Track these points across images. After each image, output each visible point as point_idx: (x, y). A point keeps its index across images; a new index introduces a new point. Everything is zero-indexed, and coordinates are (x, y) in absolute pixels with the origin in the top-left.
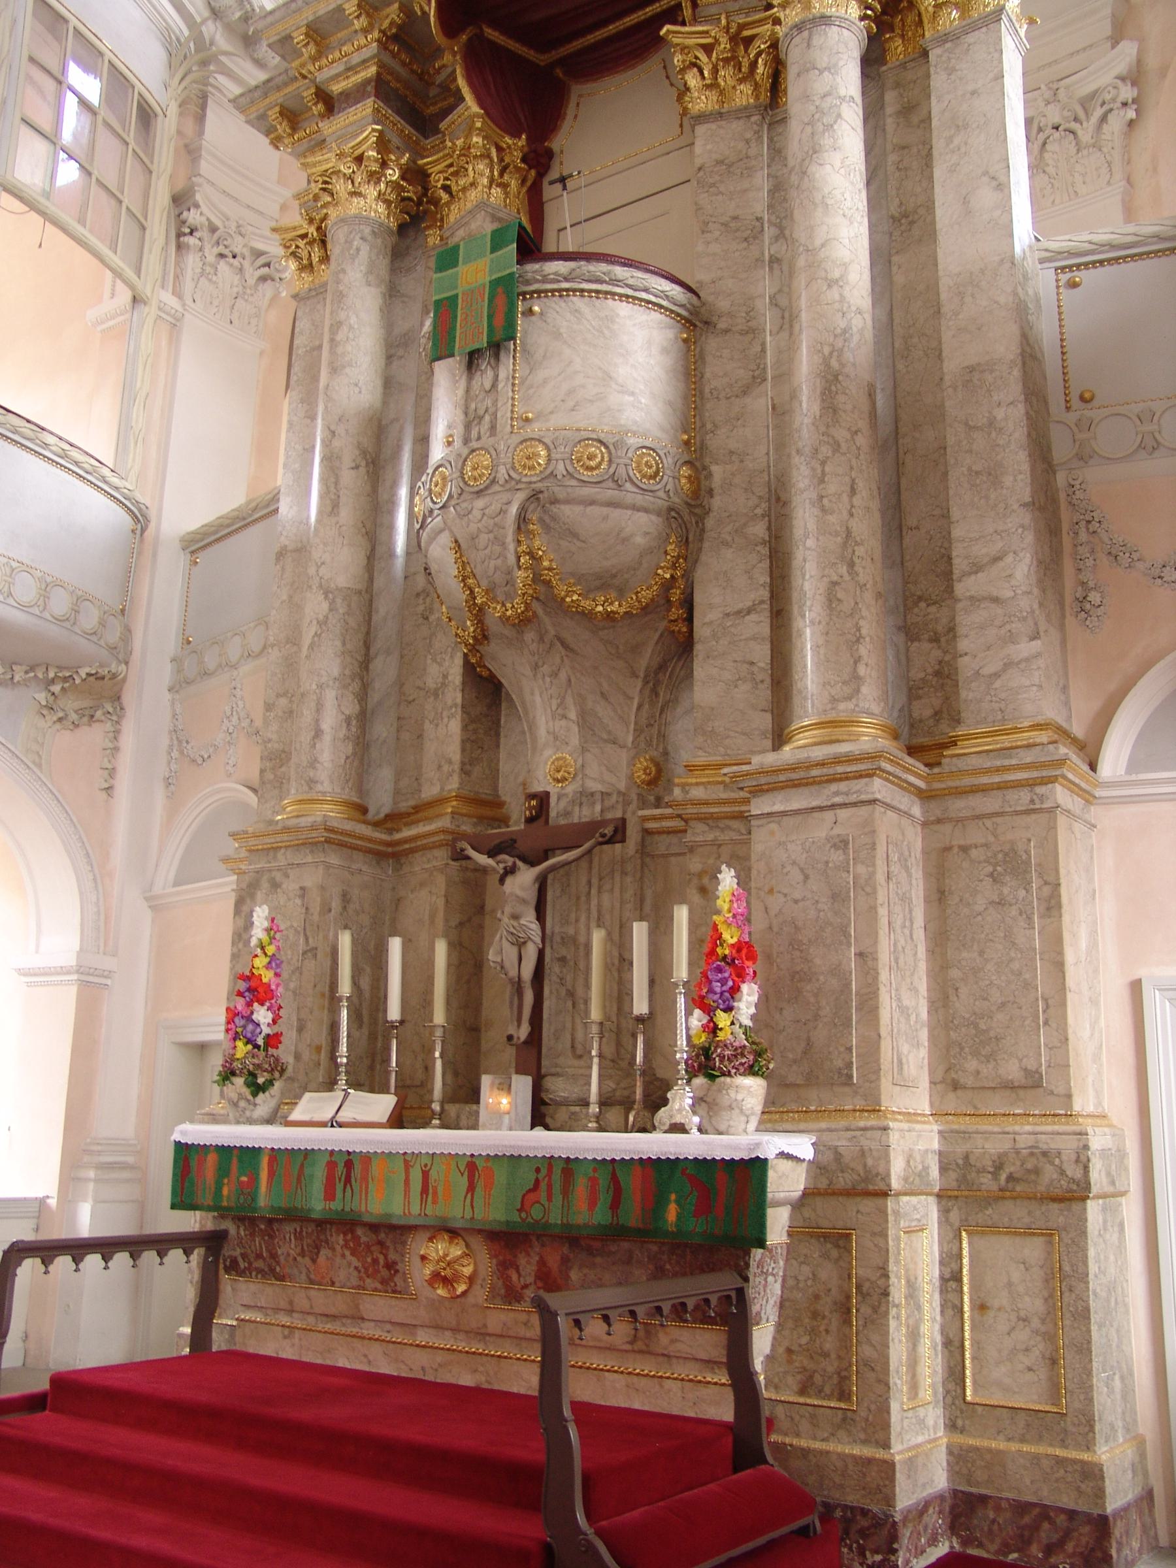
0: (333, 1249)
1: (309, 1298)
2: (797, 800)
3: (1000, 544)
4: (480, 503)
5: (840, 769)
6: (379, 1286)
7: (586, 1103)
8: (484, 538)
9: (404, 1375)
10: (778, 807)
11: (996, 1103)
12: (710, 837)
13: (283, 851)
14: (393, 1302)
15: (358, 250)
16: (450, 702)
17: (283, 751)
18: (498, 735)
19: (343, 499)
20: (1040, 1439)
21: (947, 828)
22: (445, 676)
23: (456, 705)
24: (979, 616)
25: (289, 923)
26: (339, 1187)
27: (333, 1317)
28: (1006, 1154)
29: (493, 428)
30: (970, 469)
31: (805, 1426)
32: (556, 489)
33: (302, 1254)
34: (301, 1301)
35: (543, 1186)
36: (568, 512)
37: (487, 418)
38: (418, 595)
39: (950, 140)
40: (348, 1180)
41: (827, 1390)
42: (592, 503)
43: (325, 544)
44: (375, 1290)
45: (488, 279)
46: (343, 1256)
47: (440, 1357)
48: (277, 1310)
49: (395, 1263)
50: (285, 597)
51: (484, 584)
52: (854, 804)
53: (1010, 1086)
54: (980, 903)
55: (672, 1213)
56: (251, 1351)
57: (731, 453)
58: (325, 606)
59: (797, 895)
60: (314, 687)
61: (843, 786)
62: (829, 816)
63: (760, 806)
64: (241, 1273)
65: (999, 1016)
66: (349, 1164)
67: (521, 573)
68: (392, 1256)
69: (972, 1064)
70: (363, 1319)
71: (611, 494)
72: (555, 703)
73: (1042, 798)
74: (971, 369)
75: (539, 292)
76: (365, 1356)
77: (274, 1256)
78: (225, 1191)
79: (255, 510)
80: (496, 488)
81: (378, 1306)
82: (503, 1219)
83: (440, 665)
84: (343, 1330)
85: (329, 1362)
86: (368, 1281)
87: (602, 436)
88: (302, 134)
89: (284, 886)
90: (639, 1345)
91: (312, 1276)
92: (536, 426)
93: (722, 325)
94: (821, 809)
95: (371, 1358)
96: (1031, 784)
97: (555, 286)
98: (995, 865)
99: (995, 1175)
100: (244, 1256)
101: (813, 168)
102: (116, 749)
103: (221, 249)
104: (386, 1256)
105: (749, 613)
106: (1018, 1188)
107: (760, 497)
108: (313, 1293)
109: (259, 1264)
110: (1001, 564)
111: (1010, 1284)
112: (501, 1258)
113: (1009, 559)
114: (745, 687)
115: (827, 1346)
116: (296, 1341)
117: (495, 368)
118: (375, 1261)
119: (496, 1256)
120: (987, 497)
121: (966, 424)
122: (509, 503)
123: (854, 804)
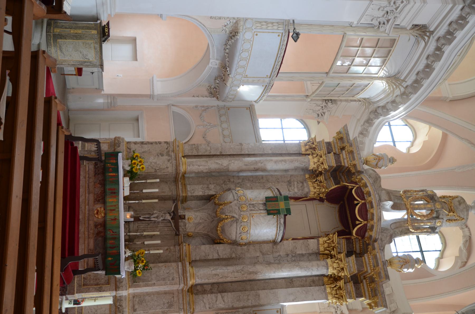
0: (101, 188)
1: (92, 182)
2: (180, 271)
3: (226, 301)
4: (237, 208)
5: (185, 279)
8: (231, 209)
9: (80, 203)
10: (180, 267)
11: (131, 304)
14: (93, 201)
15: (302, 164)
16: (205, 191)
17: (199, 150)
18: (199, 200)
19: (247, 166)
21: (177, 294)
22: (211, 190)
23: (205, 193)
24: (214, 298)
26: (110, 191)
27: (89, 187)
28: (123, 307)
29: (251, 210)
30: (240, 296)
31: (78, 279)
32: (239, 223)
33: (99, 181)
34: (91, 180)
35: (113, 233)
36: (235, 225)
37: (253, 209)
38: (229, 179)
39: (305, 291)
40: (112, 193)
41: (84, 282)
42: (237, 229)
43: (238, 164)
44: (94, 197)
45: (280, 208)
46: (100, 190)
48: (89, 174)
49: (100, 202)
50: (232, 147)
51: (223, 208)
52: (179, 281)
53: (134, 306)
54: (164, 300)
55: (110, 259)
56: (81, 169)
57: (249, 250)
58: (225, 165)
59: (165, 272)
60: (209, 164)
61: (183, 279)
62: (178, 277)
63: (180, 264)
64: (95, 166)
65: (145, 304)
66: (115, 193)
67: (224, 216)
69: (137, 300)
71: (238, 232)
72: (203, 218)
73: (181, 310)
74: (259, 296)
75: (278, 217)
77: (98, 174)
78: (109, 165)
79: (256, 128)
80: (240, 212)
81: (92, 197)
83: (213, 188)
84: (87, 190)
86: (96, 196)
87: (249, 230)
88: (338, 141)
89: (169, 163)
90: (90, 251)
92: (251, 218)
93: (274, 247)
94: (179, 275)
96: (184, 308)
97: (279, 220)
98: (170, 303)
99: (119, 305)
101: (298, 268)
102: (203, 97)
103: (324, 107)
104: (101, 199)
105: (218, 254)
106: (117, 309)
107: (240, 256)
108: (92, 183)
110: (223, 302)
113: (223, 303)
114: (204, 254)
115: (91, 282)
116: (84, 179)
117: (264, 210)
118: (99, 197)
120: (235, 299)
121: (249, 295)
122: (237, 215)
123: (179, 281)
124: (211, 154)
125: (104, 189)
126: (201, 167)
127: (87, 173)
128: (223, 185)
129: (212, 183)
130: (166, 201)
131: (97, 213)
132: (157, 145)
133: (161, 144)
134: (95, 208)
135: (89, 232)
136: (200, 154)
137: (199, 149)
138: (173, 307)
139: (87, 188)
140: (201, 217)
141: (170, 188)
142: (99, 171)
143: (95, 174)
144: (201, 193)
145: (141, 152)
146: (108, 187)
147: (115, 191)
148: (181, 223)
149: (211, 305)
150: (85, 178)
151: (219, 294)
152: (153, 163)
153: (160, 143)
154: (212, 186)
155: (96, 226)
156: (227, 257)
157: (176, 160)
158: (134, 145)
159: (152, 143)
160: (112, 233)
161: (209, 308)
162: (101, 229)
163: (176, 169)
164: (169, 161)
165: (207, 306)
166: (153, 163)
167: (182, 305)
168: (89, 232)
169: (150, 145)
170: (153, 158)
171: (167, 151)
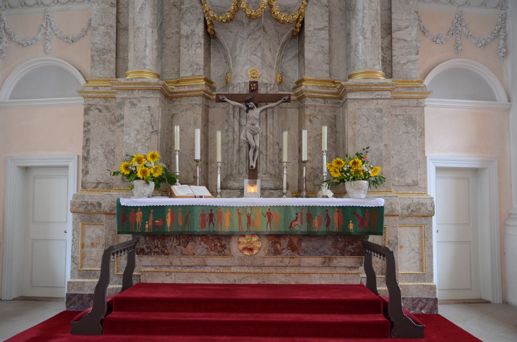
0: (196, 242)
2: (364, 96)
6: (217, 254)
7: (282, 189)
10: (357, 97)
12: (313, 103)
13: (137, 91)
16: (196, 42)
17: (104, 49)
20: (418, 281)
22: (194, 31)
23: (200, 43)
25: (143, 120)
27: (191, 266)
33: (179, 245)
34: (176, 261)
35: (299, 219)
40: (211, 220)
46: (200, 244)
47: (242, 276)
53: (408, 185)
60: (144, 26)
61: (380, 93)
62: (375, 101)
63: (350, 96)
64: (147, 254)
66: (211, 215)
68: (224, 243)
69: (397, 179)
70: (207, 266)
72: (253, 49)
76: (208, 279)
77: (164, 247)
78: (147, 226)
82: (283, 230)
83: (189, 26)
85: (191, 282)
86: (212, 252)
91: (184, 253)
95: (210, 279)
96: (417, 99)
99: (407, 210)
100: (147, 248)
104: (221, 243)
108: (182, 259)
109: (157, 250)
111: (409, 240)
112: (274, 240)
113: (410, 28)
118: (216, 245)
119: (271, 240)
124: (114, 25)
125: (198, 236)
126: (148, 43)
127: (159, 269)
128: (183, 7)
129: (177, 30)
130: (210, 119)
131: (251, 250)
132: (92, 130)
133: (91, 122)
134: (240, 254)
135: (287, 266)
136: (114, 46)
137: (103, 47)
138: (414, 116)
139: (193, 270)
140: (252, 54)
141: (187, 110)
142: (157, 247)
143: (163, 253)
144: (201, 51)
145: (106, 162)
146: (197, 228)
147: (207, 215)
148: (262, 91)
149: (411, 50)
150: (170, 273)
151: (394, 35)
152: (139, 137)
153: (87, 124)
154: (185, 29)
155: (277, 252)
156: (327, 14)
157: (132, 90)
158: (88, 176)
159: (87, 140)
160: (298, 222)
161: (417, 54)
162: (284, 243)
163: (154, 90)
164: (133, 105)
165: (413, 57)
166: (139, 137)
167: (411, 101)
168: (287, 266)
169: (92, 144)
170: (127, 137)
171: (104, 111)
